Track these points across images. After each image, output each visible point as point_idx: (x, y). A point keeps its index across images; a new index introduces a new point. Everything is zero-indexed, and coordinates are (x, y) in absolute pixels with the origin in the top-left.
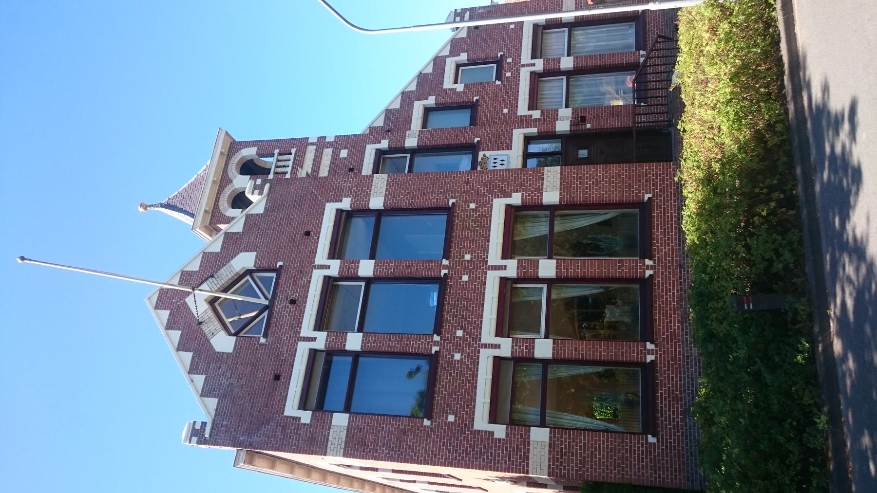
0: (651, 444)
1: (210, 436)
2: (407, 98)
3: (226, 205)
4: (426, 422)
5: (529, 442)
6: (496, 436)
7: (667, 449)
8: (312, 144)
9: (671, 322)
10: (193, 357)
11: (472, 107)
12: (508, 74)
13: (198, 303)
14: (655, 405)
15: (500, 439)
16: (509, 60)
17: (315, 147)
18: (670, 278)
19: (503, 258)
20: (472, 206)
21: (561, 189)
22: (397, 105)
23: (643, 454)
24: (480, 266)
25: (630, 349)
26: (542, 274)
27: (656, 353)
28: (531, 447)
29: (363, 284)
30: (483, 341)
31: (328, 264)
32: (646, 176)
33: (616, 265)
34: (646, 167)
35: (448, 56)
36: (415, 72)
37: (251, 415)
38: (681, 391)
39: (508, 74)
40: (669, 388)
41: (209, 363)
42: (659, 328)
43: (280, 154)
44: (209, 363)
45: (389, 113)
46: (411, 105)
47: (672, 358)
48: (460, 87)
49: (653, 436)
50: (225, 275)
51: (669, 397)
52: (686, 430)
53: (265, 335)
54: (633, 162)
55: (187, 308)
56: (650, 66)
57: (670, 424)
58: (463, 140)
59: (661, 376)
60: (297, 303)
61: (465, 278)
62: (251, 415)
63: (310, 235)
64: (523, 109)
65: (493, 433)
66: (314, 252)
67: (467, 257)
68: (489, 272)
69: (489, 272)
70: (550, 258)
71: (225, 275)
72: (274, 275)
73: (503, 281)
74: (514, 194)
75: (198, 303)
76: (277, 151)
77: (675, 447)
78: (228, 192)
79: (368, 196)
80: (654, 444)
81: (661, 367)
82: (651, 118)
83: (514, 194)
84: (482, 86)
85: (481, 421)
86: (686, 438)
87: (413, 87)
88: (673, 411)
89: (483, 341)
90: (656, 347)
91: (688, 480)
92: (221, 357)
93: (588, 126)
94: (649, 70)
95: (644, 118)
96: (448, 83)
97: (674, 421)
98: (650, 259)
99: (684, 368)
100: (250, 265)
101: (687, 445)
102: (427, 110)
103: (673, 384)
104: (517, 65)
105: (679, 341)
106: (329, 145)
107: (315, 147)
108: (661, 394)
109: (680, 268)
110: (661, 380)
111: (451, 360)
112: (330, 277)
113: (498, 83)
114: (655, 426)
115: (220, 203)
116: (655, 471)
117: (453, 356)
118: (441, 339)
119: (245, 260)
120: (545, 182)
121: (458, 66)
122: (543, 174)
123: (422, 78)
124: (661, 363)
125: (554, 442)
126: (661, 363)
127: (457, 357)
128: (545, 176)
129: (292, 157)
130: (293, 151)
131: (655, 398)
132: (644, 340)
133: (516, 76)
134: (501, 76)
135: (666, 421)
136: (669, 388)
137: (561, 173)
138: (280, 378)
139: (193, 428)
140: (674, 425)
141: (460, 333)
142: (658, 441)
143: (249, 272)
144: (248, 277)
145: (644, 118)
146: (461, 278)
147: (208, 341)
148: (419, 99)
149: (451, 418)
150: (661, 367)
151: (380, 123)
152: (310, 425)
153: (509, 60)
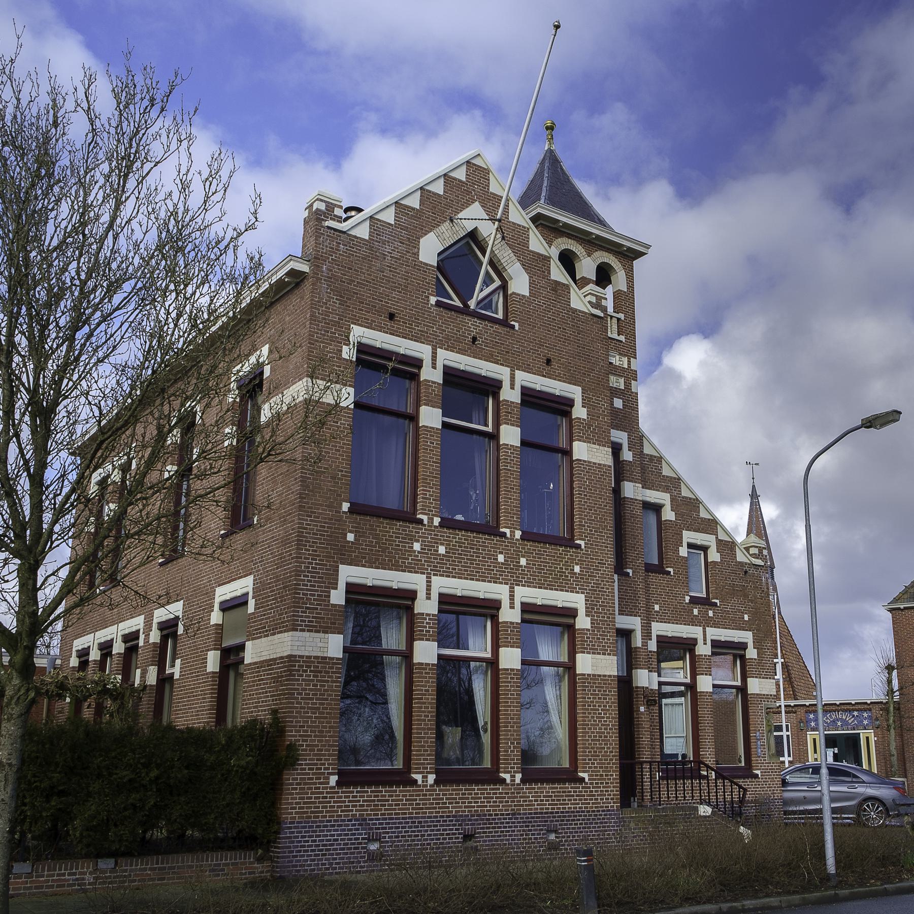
0: (328, 778)
1: (328, 227)
2: (673, 484)
3: (563, 247)
4: (346, 506)
5: (327, 632)
6: (332, 591)
7: (323, 798)
8: (629, 362)
9: (456, 803)
10: (413, 209)
11: (659, 569)
12: (696, 612)
13: (473, 216)
14: (369, 784)
15: (329, 596)
16: (711, 613)
17: (626, 366)
18: (502, 802)
19: (441, 595)
20: (577, 569)
21: (594, 675)
22: (666, 472)
23: (317, 769)
24: (514, 577)
25: (428, 755)
26: (418, 645)
27: (424, 786)
28: (321, 635)
29: (490, 429)
30: (434, 578)
31: (516, 387)
32: (606, 775)
33: (515, 739)
34: (615, 775)
35: (717, 538)
36: (702, 496)
37: (351, 282)
38: (384, 814)
39: (696, 612)
40: (388, 801)
41: (406, 229)
42: (451, 790)
43: (619, 319)
44: (406, 229)
45: (659, 459)
46: (666, 489)
47: (419, 804)
48: (683, 551)
49: (337, 782)
50: (506, 256)
51: (378, 801)
52: (344, 821)
53: (438, 304)
54: (620, 759)
55: (467, 204)
56: (700, 783)
57: (349, 801)
58: (631, 555)
59: (357, 792)
60: (472, 346)
61: (501, 558)
62: (351, 282)
63: (547, 367)
64: (659, 628)
65: (336, 588)
66: (528, 370)
67: (523, 561)
68: (507, 587)
69: (507, 587)
70: (345, 650)
71: (506, 256)
72: (500, 316)
73: (412, 595)
74: (589, 619)
75: (473, 216)
76: (621, 316)
77: (326, 807)
78: (577, 248)
79: (588, 440)
80: (328, 783)
81: (409, 791)
82: (647, 784)
83: (589, 619)
84: (685, 582)
85: (348, 573)
86: (335, 821)
87: (685, 493)
88: (363, 806)
89: (434, 578)
90: (431, 786)
91: (290, 823)
92: (414, 244)
93: (642, 709)
94: (696, 782)
95: (647, 775)
96: (689, 536)
97: (353, 806)
98: (522, 780)
99: (409, 818)
100: (513, 288)
101: (328, 821)
102: (657, 508)
103: (392, 805)
104: (706, 622)
105: (436, 812)
106: (628, 385)
107: (626, 366)
108: (381, 792)
109: (513, 814)
110: (353, 792)
111: (414, 539)
112: (500, 388)
113: (687, 599)
114: (348, 785)
115: (565, 239)
116: (300, 784)
117: (418, 541)
118: (436, 527)
119: (520, 284)
120: (601, 656)
121: (705, 549)
122: (609, 654)
123: (694, 504)
124: (414, 791)
125: (329, 663)
126: (414, 791)
127: (417, 546)
128: (607, 657)
129: (615, 336)
130: (622, 338)
131: (377, 784)
132: (340, 773)
133: (693, 621)
134: (694, 603)
135: (353, 797)
136: (388, 801)
137: (610, 676)
138: (391, 320)
139: (336, 205)
140: (348, 806)
141: (442, 550)
142: (332, 788)
143: (504, 287)
144: (498, 283)
145: (647, 775)
146: (501, 553)
147: (431, 230)
148: (673, 500)
149: (350, 537)
150: (409, 791)
151: (647, 450)
152: (340, 358)
153: (711, 613)
